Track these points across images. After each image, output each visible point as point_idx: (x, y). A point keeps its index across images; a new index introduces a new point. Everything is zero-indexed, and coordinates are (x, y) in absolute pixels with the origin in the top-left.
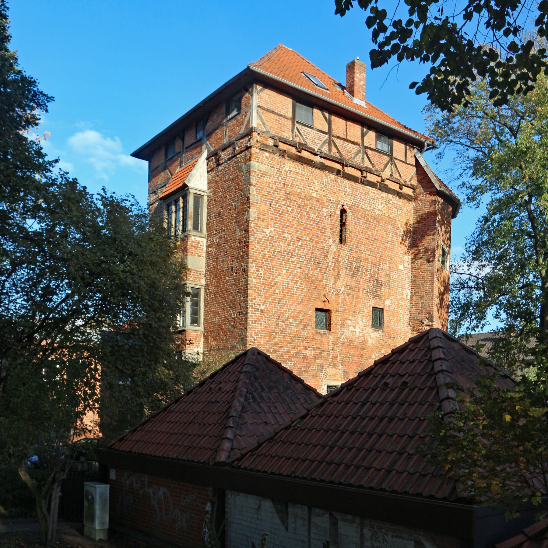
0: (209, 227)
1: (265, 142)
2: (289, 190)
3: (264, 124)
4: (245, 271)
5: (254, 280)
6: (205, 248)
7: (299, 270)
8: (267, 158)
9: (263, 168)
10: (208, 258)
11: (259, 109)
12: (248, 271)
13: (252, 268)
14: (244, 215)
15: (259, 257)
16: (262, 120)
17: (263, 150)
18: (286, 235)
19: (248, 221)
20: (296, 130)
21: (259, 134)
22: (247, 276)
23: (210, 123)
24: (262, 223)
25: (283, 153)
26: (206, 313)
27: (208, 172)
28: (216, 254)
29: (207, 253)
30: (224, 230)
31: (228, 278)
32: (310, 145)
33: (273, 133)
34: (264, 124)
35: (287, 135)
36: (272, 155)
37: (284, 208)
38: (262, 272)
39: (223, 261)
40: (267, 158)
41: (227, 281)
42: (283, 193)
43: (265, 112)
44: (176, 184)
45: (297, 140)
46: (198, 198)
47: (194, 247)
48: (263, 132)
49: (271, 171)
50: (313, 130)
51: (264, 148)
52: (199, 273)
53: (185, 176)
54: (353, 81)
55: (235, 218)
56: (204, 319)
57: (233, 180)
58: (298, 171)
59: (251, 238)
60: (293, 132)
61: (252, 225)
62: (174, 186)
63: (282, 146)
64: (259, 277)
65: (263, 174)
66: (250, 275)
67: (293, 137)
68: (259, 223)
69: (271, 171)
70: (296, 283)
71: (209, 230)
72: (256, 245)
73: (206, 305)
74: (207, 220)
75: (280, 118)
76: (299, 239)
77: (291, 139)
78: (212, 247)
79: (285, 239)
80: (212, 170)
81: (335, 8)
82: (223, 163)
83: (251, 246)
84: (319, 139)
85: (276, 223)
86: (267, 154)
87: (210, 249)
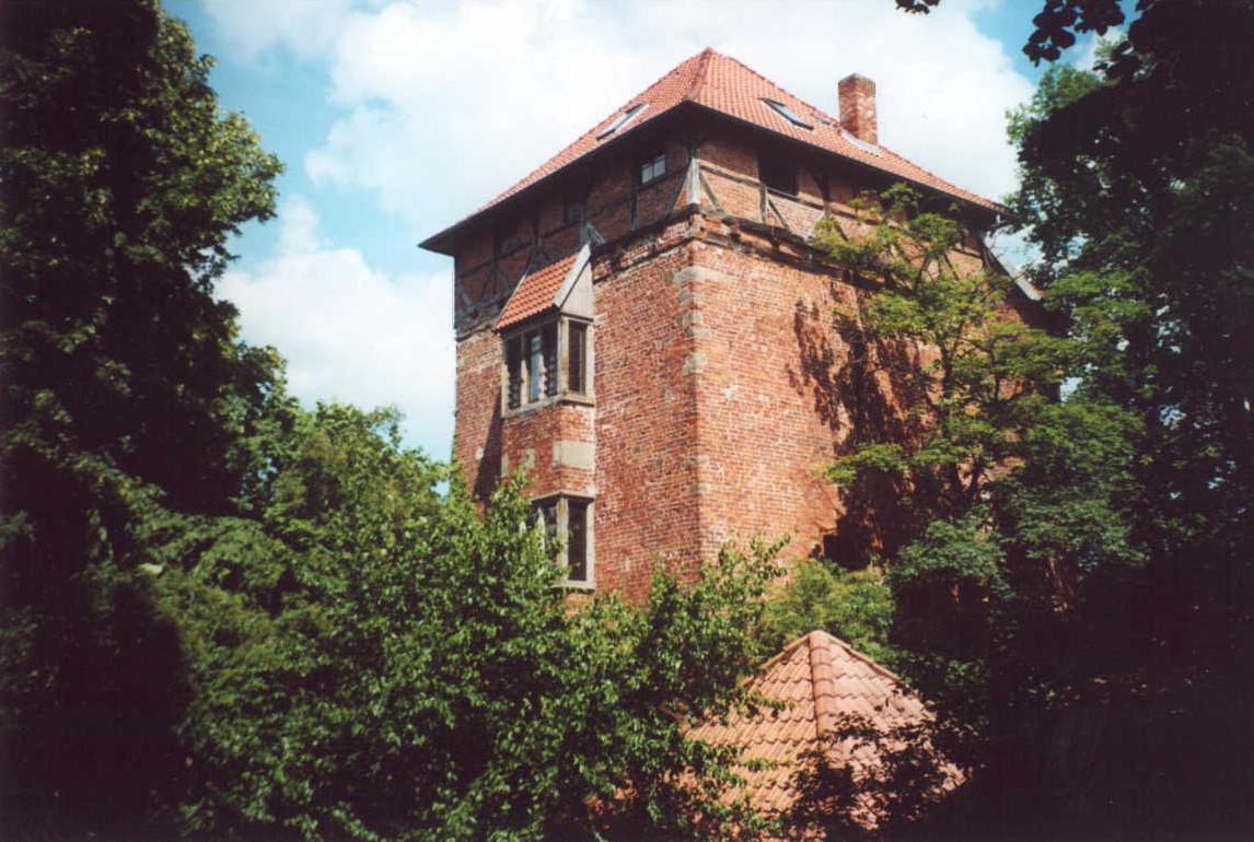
0: (602, 386)
1: (715, 229)
2: (762, 314)
3: (712, 197)
4: (692, 469)
5: (709, 486)
6: (592, 425)
7: (788, 463)
8: (720, 257)
9: (714, 276)
10: (601, 444)
11: (704, 173)
12: (696, 469)
13: (705, 462)
14: (681, 363)
15: (716, 442)
16: (708, 191)
17: (710, 243)
18: (761, 398)
19: (691, 375)
20: (768, 206)
21: (704, 216)
22: (696, 478)
23: (598, 193)
24: (718, 378)
25: (748, 249)
26: (600, 553)
27: (595, 282)
28: (619, 436)
29: (600, 435)
30: (637, 392)
31: (648, 483)
32: (795, 230)
33: (729, 213)
34: (712, 197)
35: (753, 214)
36: (729, 252)
37: (754, 347)
38: (722, 470)
39: (637, 450)
40: (720, 257)
41: (647, 489)
42: (750, 322)
43: (714, 176)
44: (530, 305)
45: (771, 222)
46: (578, 327)
47: (573, 423)
48: (711, 212)
49: (727, 280)
50: (797, 205)
51: (714, 239)
52: (583, 473)
53: (551, 289)
54: (855, 111)
55: (662, 368)
56: (597, 566)
57: (651, 298)
58: (775, 278)
59: (700, 406)
60: (763, 210)
61: (700, 382)
62: (521, 308)
63: (745, 237)
64: (716, 480)
65: (715, 287)
66: (702, 477)
67: (764, 219)
68: (713, 377)
69: (727, 280)
70: (784, 488)
71: (600, 388)
72: (708, 419)
73: (600, 537)
74: (597, 372)
75: (741, 185)
76: (784, 404)
77: (760, 221)
78: (609, 422)
79: (759, 405)
80: (603, 279)
81: (1026, 42)
82: (627, 268)
83: (700, 423)
84: (809, 218)
85: (742, 377)
86: (720, 251)
87: (605, 427)
